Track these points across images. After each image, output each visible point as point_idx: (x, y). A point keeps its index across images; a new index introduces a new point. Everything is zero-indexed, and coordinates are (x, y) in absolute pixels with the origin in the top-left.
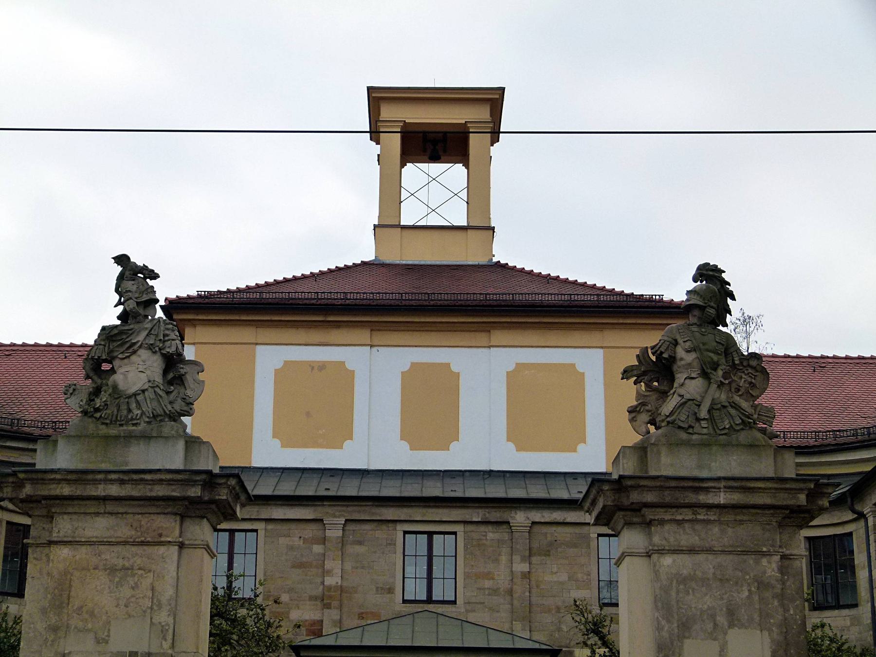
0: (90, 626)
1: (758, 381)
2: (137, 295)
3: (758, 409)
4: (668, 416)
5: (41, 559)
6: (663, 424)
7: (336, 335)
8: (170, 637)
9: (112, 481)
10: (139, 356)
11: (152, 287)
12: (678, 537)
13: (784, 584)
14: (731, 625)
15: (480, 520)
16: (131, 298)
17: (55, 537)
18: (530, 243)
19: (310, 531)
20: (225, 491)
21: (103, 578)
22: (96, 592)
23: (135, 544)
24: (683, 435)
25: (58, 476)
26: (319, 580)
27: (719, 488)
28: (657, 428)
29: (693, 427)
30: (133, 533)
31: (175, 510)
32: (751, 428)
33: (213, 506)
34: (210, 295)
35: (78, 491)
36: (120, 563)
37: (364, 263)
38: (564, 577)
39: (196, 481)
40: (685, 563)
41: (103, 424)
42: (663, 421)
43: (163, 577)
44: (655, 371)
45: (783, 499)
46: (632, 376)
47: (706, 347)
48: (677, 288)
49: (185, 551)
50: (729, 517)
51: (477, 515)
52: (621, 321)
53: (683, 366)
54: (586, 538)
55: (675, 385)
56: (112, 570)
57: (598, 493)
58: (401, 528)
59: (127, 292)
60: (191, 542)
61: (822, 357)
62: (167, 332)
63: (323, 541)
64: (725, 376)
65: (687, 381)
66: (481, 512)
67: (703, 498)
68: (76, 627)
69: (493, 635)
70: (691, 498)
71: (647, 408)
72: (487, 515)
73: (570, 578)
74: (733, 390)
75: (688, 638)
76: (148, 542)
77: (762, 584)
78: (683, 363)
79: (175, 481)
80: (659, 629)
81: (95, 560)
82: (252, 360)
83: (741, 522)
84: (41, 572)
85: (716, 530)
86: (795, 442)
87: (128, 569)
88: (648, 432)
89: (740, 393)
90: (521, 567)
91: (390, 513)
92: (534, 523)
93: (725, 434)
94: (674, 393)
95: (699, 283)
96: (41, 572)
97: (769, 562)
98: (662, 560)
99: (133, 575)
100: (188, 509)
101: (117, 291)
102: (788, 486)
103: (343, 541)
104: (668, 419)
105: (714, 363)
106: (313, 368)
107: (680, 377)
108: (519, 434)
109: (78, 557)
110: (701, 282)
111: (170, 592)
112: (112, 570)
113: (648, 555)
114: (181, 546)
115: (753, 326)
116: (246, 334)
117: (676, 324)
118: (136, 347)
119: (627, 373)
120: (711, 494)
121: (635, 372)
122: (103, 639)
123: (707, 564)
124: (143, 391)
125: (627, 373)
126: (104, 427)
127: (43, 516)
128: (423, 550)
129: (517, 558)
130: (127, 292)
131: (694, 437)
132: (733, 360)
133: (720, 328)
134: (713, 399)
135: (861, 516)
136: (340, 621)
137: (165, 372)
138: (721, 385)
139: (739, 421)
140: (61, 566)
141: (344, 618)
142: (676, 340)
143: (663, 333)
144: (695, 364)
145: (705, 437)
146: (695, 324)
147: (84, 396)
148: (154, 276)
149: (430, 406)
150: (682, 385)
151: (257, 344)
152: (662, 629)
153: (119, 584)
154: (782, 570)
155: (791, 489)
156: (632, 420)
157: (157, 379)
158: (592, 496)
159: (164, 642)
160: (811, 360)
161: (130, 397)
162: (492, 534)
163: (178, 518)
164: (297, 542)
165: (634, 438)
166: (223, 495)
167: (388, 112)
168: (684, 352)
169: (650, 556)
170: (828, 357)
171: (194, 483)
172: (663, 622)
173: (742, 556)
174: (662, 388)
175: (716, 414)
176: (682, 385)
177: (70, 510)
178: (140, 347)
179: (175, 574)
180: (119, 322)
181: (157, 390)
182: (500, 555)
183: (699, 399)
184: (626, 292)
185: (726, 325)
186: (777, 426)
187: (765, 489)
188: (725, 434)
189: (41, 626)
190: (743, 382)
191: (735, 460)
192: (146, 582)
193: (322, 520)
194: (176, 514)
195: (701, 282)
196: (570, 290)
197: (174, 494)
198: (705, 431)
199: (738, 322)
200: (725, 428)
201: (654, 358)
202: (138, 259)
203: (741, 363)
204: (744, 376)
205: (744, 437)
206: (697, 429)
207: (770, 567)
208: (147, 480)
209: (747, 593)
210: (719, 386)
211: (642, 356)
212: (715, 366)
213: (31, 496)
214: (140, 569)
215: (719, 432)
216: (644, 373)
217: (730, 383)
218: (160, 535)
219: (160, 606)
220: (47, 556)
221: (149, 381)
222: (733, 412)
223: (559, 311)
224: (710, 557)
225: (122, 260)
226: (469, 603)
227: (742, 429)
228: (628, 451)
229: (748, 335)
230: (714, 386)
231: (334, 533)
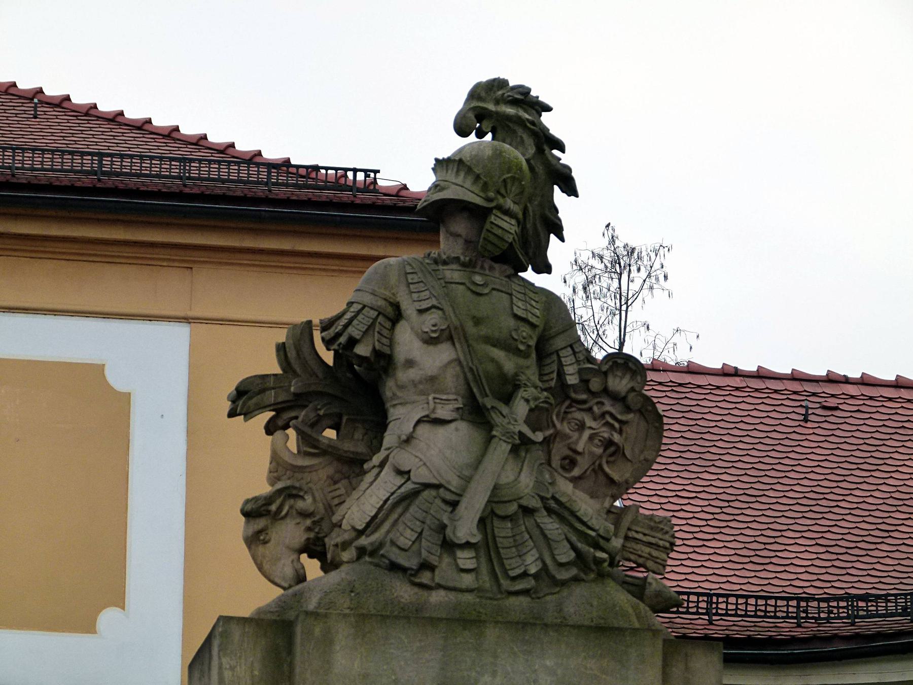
1: (630, 439)
3: (626, 523)
4: (360, 533)
6: (346, 556)
24: (404, 592)
28: (328, 566)
29: (432, 568)
32: (602, 576)
42: (345, 545)
44: (330, 396)
46: (262, 408)
47: (484, 331)
48: (407, 146)
52: (249, 242)
53: (415, 384)
55: (389, 439)
61: (831, 379)
64: (536, 418)
65: (424, 431)
71: (300, 504)
74: (556, 462)
78: (413, 374)
86: (739, 627)
88: (301, 578)
89: (576, 472)
93: (526, 592)
94: (382, 465)
95: (473, 138)
104: (364, 541)
105: (503, 378)
107: (402, 418)
110: (480, 135)
115: (638, 278)
117: (397, 257)
119: (244, 400)
121: (271, 397)
125: (244, 400)
131: (437, 597)
132: (561, 375)
133: (529, 275)
134: (496, 488)
138: (520, 446)
139: (566, 555)
142: (397, 307)
143: (359, 282)
144: (451, 379)
145: (469, 597)
146: (457, 259)
150: (409, 440)
156: (254, 540)
160: (796, 386)
165: (254, 594)
168: (417, 344)
170: (846, 380)
174: (348, 446)
175: (503, 530)
176: (409, 440)
183: (454, 483)
184: (269, 154)
185: (544, 268)
186: (675, 577)
188: (526, 592)
190: (585, 434)
195: (480, 135)
196: (98, 139)
198: (467, 580)
199: (596, 263)
200: (525, 575)
201: (328, 357)
203: (585, 382)
204: (589, 422)
205: (579, 602)
206: (445, 572)
210: (515, 450)
211: (295, 349)
212: (507, 390)
215: (505, 584)
216: (299, 400)
217: (547, 441)
222: (552, 526)
223: (62, 205)
227: (576, 579)
228: (236, 632)
229: (624, 303)
230: (501, 449)
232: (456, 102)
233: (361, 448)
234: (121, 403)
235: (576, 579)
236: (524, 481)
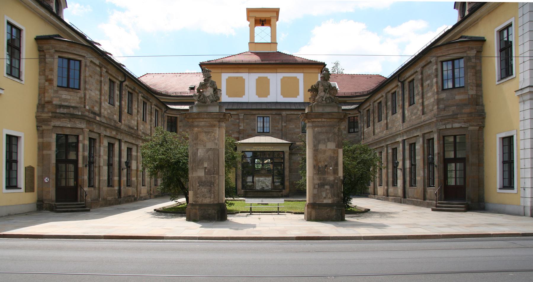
7: (240, 70)
19: (236, 117)
21: (204, 134)
38: (294, 126)
51: (274, 112)
56: (206, 132)
63: (239, 119)
77: (334, 134)
80: (314, 142)
90: (284, 124)
91: (254, 112)
103: (243, 119)
108: (284, 94)
112: (206, 132)
116: (219, 71)
119: (309, 91)
123: (324, 129)
128: (262, 120)
135: (360, 112)
147: (197, 97)
149: (263, 87)
162: (277, 117)
231: (241, 117)
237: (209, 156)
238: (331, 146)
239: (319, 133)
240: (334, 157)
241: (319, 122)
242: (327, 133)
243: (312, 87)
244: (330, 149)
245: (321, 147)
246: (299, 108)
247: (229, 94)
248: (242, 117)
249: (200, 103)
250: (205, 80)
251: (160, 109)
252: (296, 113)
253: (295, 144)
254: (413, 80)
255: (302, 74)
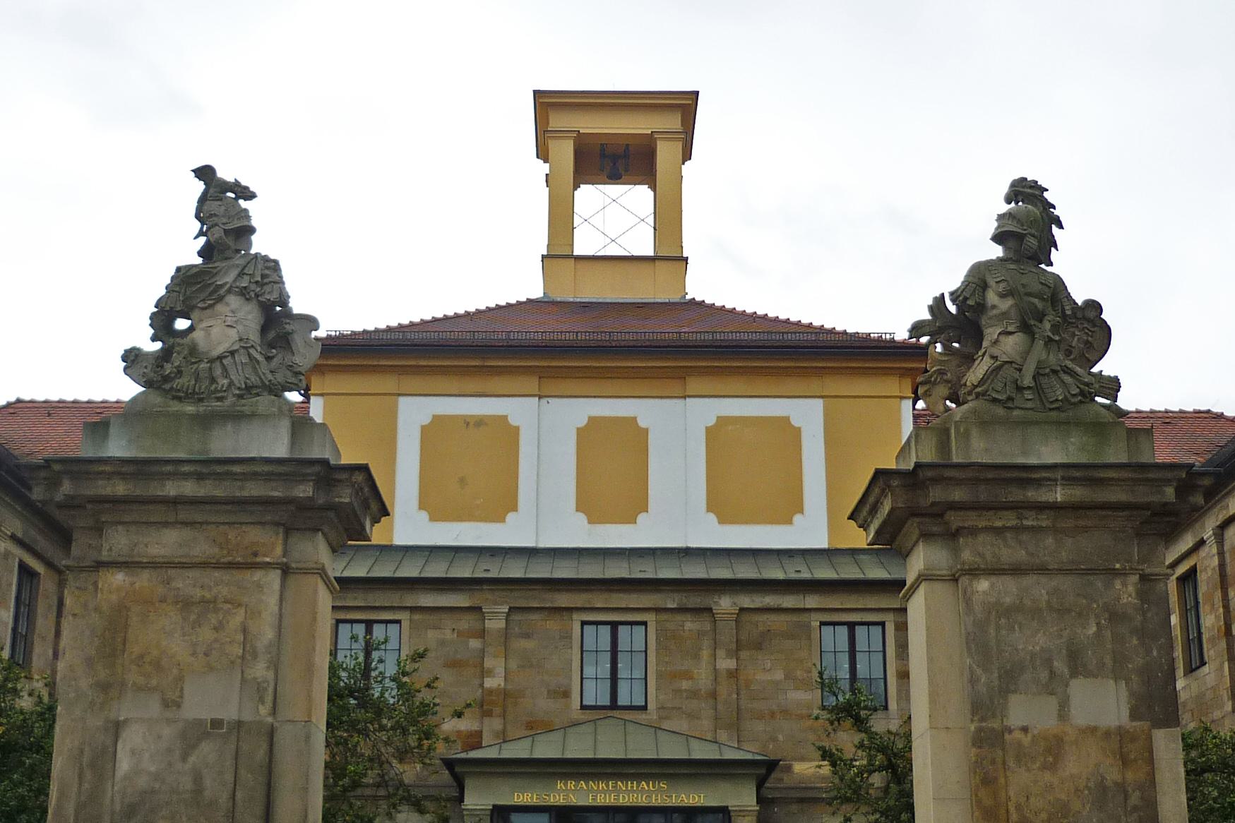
0: (154, 682)
2: (225, 220)
4: (976, 387)
5: (86, 589)
6: (970, 398)
8: (269, 699)
9: (186, 476)
10: (227, 304)
11: (246, 211)
12: (997, 550)
13: (1144, 614)
14: (1074, 673)
15: (675, 606)
16: (216, 225)
17: (105, 556)
18: (730, 272)
19: (466, 622)
20: (348, 491)
22: (165, 635)
23: (219, 566)
24: (1000, 411)
25: (108, 468)
26: (477, 682)
27: (1056, 480)
28: (958, 404)
30: (217, 550)
31: (277, 518)
33: (331, 514)
34: (342, 336)
35: (138, 490)
36: (198, 593)
37: (529, 301)
38: (779, 675)
39: (304, 475)
40: (1008, 589)
41: (174, 398)
42: (970, 393)
43: (260, 613)
45: (1143, 495)
49: (292, 580)
50: (1069, 523)
54: (808, 626)
55: (985, 344)
56: (186, 604)
57: (883, 491)
58: (578, 618)
59: (211, 216)
60: (299, 565)
62: (267, 272)
63: (482, 634)
64: (1055, 328)
65: (1002, 338)
66: (677, 596)
67: (1032, 494)
68: (134, 684)
69: (695, 744)
70: (1016, 495)
72: (685, 600)
73: (787, 677)
75: (1015, 692)
76: (239, 563)
77: (1115, 616)
78: (995, 312)
79: (276, 474)
80: (973, 681)
81: (161, 590)
82: (396, 405)
83: (1085, 529)
84: (85, 606)
85: (1050, 541)
87: (209, 602)
90: (726, 664)
91: (563, 600)
92: (742, 610)
94: (983, 355)
95: (1013, 204)
96: (85, 606)
97: (1124, 584)
98: (975, 584)
99: (216, 610)
100: (296, 519)
101: (197, 217)
102: (1151, 475)
103: (506, 634)
104: (979, 389)
106: (468, 424)
107: (991, 333)
109: (137, 585)
110: (1017, 203)
111: (269, 634)
112: (186, 604)
113: (955, 580)
114: (286, 571)
116: (387, 383)
118: (222, 292)
120: (1044, 489)
122: (173, 701)
123: (1039, 589)
124: (232, 353)
126: (175, 402)
127: (91, 529)
129: (721, 653)
130: (211, 216)
131: (1016, 413)
132: (1063, 310)
133: (1043, 266)
136: (504, 731)
137: (264, 329)
140: (114, 597)
141: (509, 728)
144: (1013, 313)
148: (249, 195)
149: (614, 470)
151: (399, 395)
152: (978, 680)
153: (197, 624)
154: (1143, 595)
155: (1152, 480)
157: (251, 337)
158: (872, 499)
159: (261, 707)
161: (211, 361)
162: (690, 625)
163: (281, 530)
164: (448, 635)
166: (345, 496)
167: (558, 121)
169: (956, 580)
171: (303, 478)
172: (979, 671)
173: (1087, 577)
175: (1044, 381)
176: (996, 342)
177: (127, 518)
178: (229, 291)
179: (276, 608)
180: (199, 261)
181: (251, 351)
182: (700, 649)
183: (1019, 360)
187: (1119, 480)
189: (84, 683)
191: (1073, 444)
192: (238, 618)
193: (480, 608)
194: (277, 524)
197: (276, 494)
198: (1029, 405)
202: (225, 173)
206: (1018, 403)
207: (1126, 592)
208: (236, 474)
209: (1095, 629)
210: (1046, 344)
212: (1040, 317)
213: (72, 497)
214: (226, 602)
218: (255, 554)
219: (255, 655)
220: (95, 584)
221: (241, 340)
224: (1043, 579)
225: (205, 173)
226: (663, 708)
230: (1040, 344)
231: (495, 624)
232: (1005, 189)
233: (972, 350)
234: (798, 431)
235: (1081, 402)
236: (1055, 359)
237: (198, 778)
238: (1102, 703)
239: (1007, 613)
240: (1122, 788)
241: (999, 531)
242: (1062, 611)
243: (938, 306)
244: (1093, 730)
245: (1027, 713)
246: (805, 575)
247: (435, 504)
248: (502, 624)
249: (156, 399)
250: (204, 252)
251: (49, 564)
252: (789, 601)
253: (789, 769)
254: (1193, 570)
255: (819, 403)
